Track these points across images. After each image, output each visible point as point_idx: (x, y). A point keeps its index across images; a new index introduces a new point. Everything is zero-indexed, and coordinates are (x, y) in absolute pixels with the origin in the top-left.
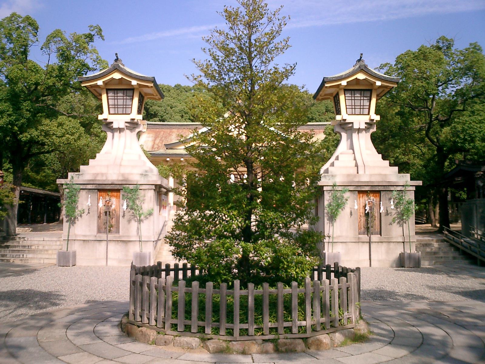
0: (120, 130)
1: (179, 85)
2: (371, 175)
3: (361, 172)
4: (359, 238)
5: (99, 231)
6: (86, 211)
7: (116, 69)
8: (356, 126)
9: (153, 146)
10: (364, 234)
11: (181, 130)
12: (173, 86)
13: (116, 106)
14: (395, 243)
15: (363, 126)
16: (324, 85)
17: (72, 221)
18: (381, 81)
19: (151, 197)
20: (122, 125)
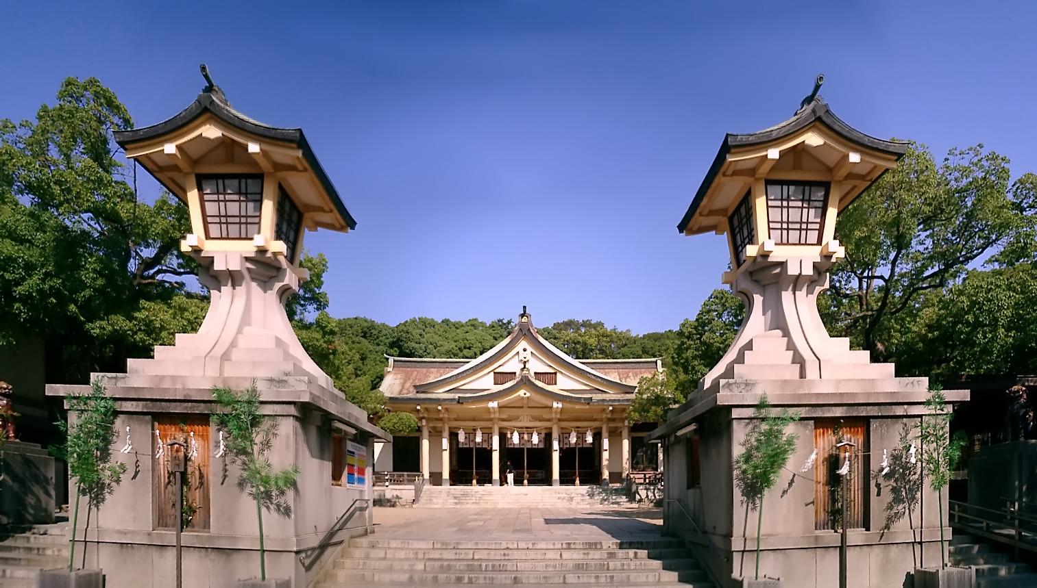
0: (233, 278)
1: (448, 320)
2: (839, 382)
3: (812, 373)
4: (817, 537)
5: (161, 520)
6: (131, 472)
7: (205, 111)
8: (793, 270)
9: (401, 391)
10: (824, 526)
11: (443, 369)
12: (440, 321)
13: (224, 219)
14: (900, 546)
15: (808, 271)
16: (725, 158)
17: (96, 491)
18: (861, 152)
19: (288, 437)
20: (235, 266)
